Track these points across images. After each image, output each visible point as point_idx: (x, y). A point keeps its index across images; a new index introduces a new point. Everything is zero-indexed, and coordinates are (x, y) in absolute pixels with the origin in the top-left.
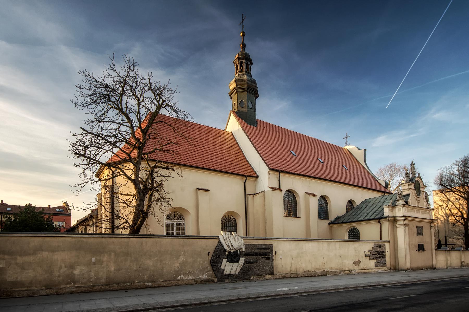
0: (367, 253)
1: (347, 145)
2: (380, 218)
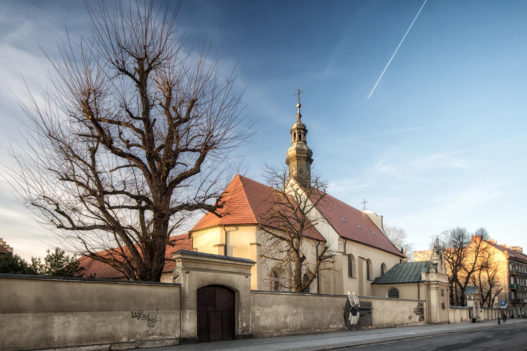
0: (415, 310)
1: (365, 209)
2: (419, 282)
